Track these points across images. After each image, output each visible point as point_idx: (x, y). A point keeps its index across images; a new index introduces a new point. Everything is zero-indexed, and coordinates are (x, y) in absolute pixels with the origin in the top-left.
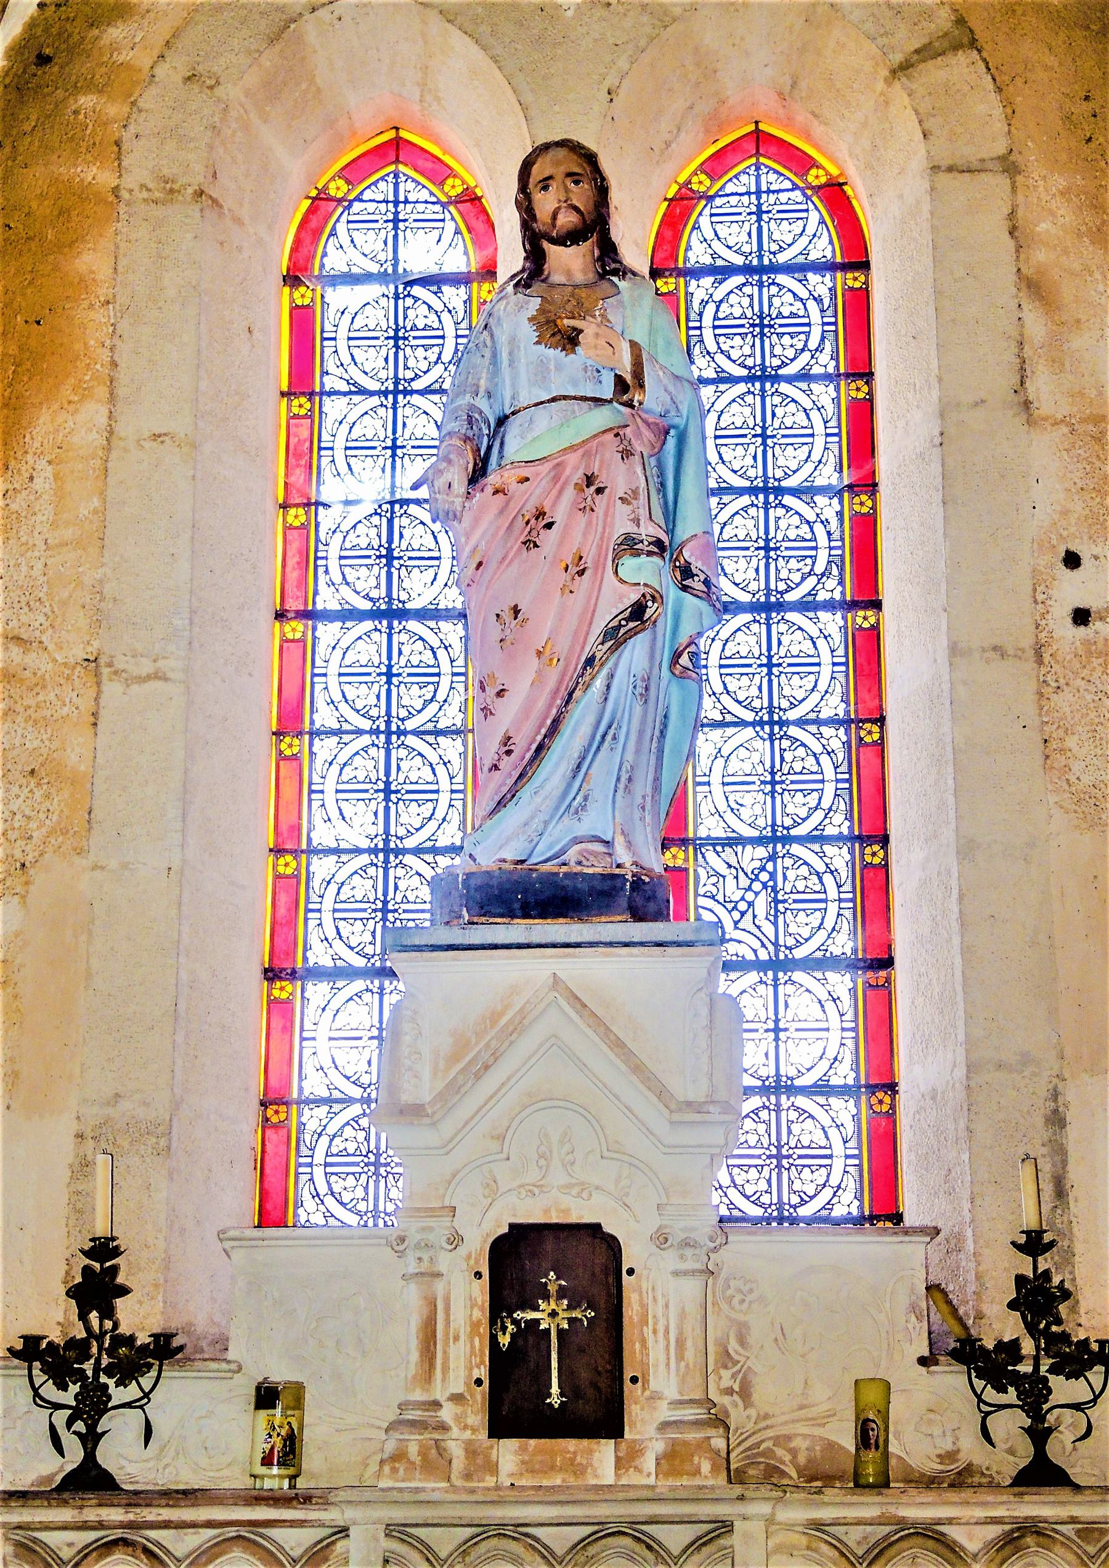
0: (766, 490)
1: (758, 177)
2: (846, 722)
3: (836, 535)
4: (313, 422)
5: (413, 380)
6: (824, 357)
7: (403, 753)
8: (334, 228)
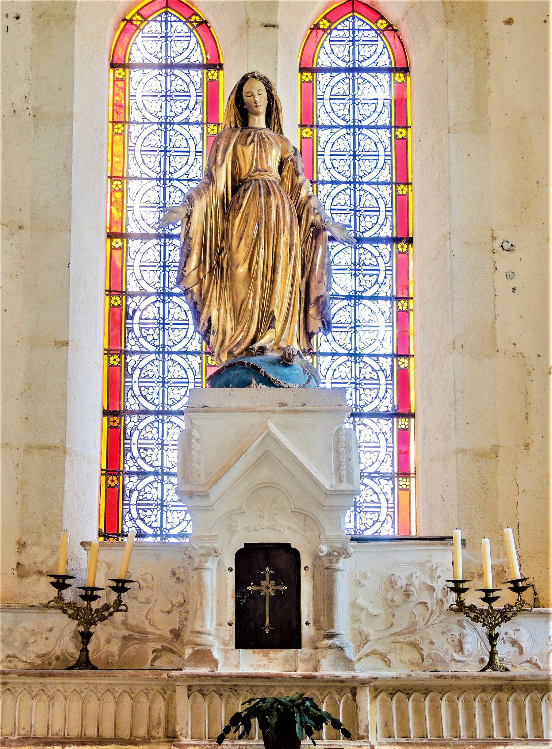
0: (354, 127)
1: (354, 23)
2: (390, 128)
3: (391, 501)
4: (123, 252)
5: (174, 117)
6: (386, 288)
7: (172, 133)
8: (135, 40)
